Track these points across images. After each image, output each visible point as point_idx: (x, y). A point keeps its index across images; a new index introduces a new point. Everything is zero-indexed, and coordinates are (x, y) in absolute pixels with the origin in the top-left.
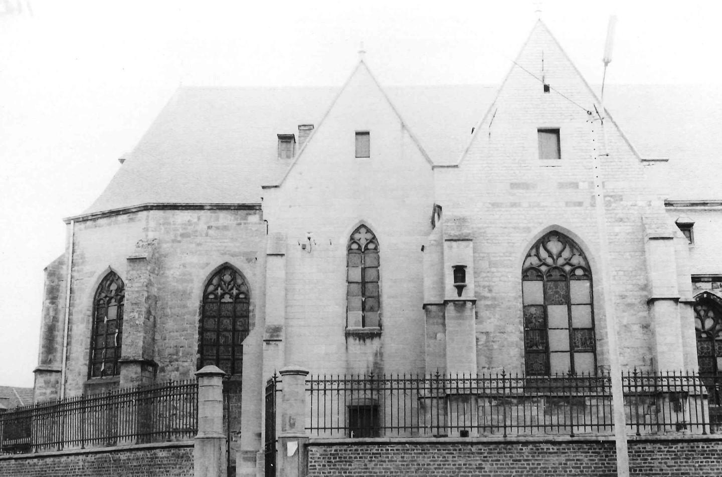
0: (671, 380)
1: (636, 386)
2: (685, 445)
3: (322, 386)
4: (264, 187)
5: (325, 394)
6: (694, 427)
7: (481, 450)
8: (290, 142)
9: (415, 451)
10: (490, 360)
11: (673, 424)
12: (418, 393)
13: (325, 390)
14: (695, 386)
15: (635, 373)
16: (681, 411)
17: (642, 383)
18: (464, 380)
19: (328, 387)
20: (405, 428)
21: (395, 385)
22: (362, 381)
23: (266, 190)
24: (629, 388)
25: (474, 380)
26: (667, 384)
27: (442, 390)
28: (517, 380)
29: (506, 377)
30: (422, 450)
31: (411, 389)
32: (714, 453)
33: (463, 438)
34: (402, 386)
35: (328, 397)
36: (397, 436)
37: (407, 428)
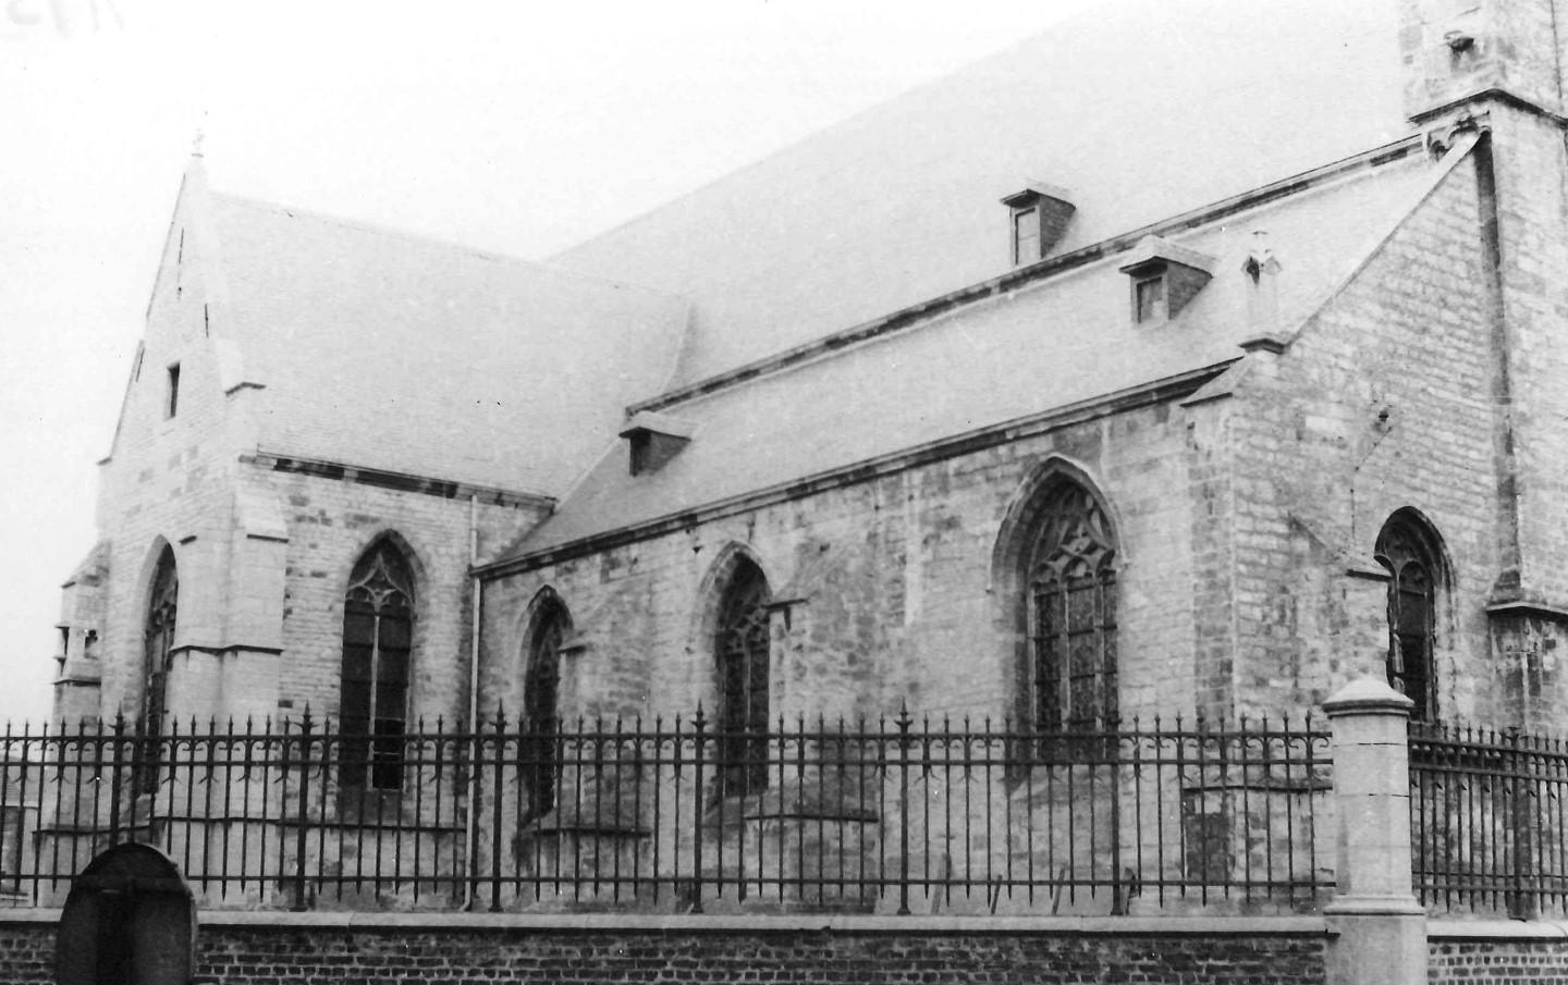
0: (975, 744)
1: (1201, 763)
2: (852, 942)
3: (239, 754)
4: (175, 372)
5: (678, 774)
6: (233, 887)
7: (1515, 960)
8: (1160, 279)
9: (1145, 961)
10: (642, 692)
11: (268, 878)
12: (1181, 775)
13: (210, 765)
14: (801, 763)
16: (975, 838)
17: (801, 753)
18: (968, 737)
19: (258, 755)
20: (243, 879)
21: (937, 753)
22: (430, 738)
23: (165, 375)
24: (1267, 766)
25: (1189, 736)
26: (962, 758)
27: (834, 768)
28: (988, 739)
29: (910, 730)
30: (350, 950)
31: (1160, 763)
32: (555, 968)
33: (1246, 919)
34: (89, 756)
35: (978, 788)
36: (1026, 910)
37: (808, 882)
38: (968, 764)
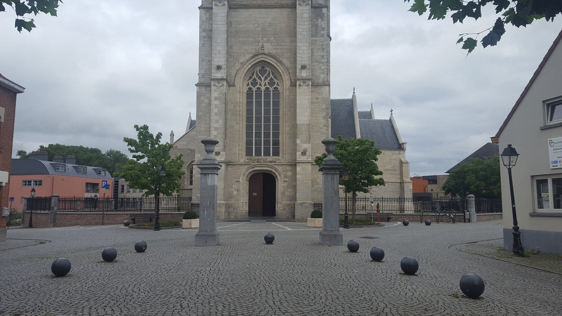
15: (75, 197)
38: (377, 201)
